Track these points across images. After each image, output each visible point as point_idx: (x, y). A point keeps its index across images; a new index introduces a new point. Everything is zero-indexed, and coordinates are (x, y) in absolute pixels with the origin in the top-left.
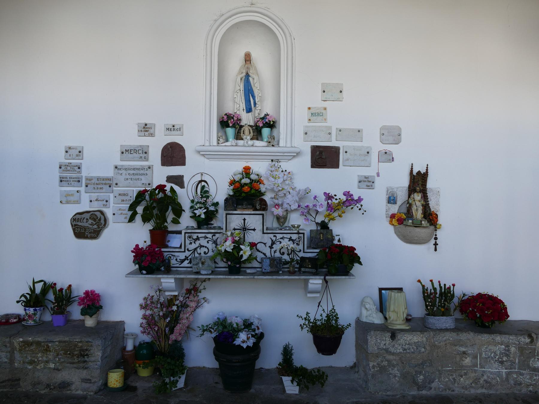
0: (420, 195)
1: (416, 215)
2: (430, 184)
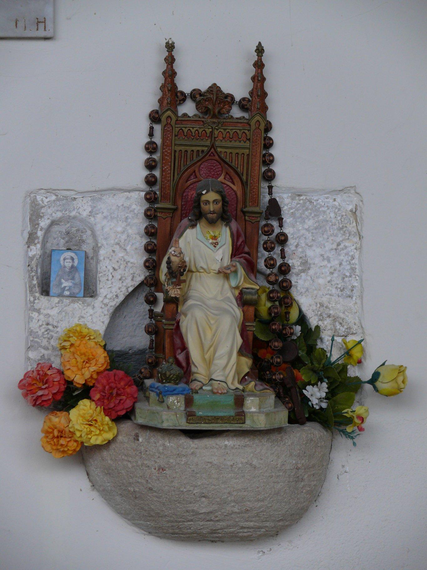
0: (225, 235)
1: (209, 363)
2: (299, 165)
